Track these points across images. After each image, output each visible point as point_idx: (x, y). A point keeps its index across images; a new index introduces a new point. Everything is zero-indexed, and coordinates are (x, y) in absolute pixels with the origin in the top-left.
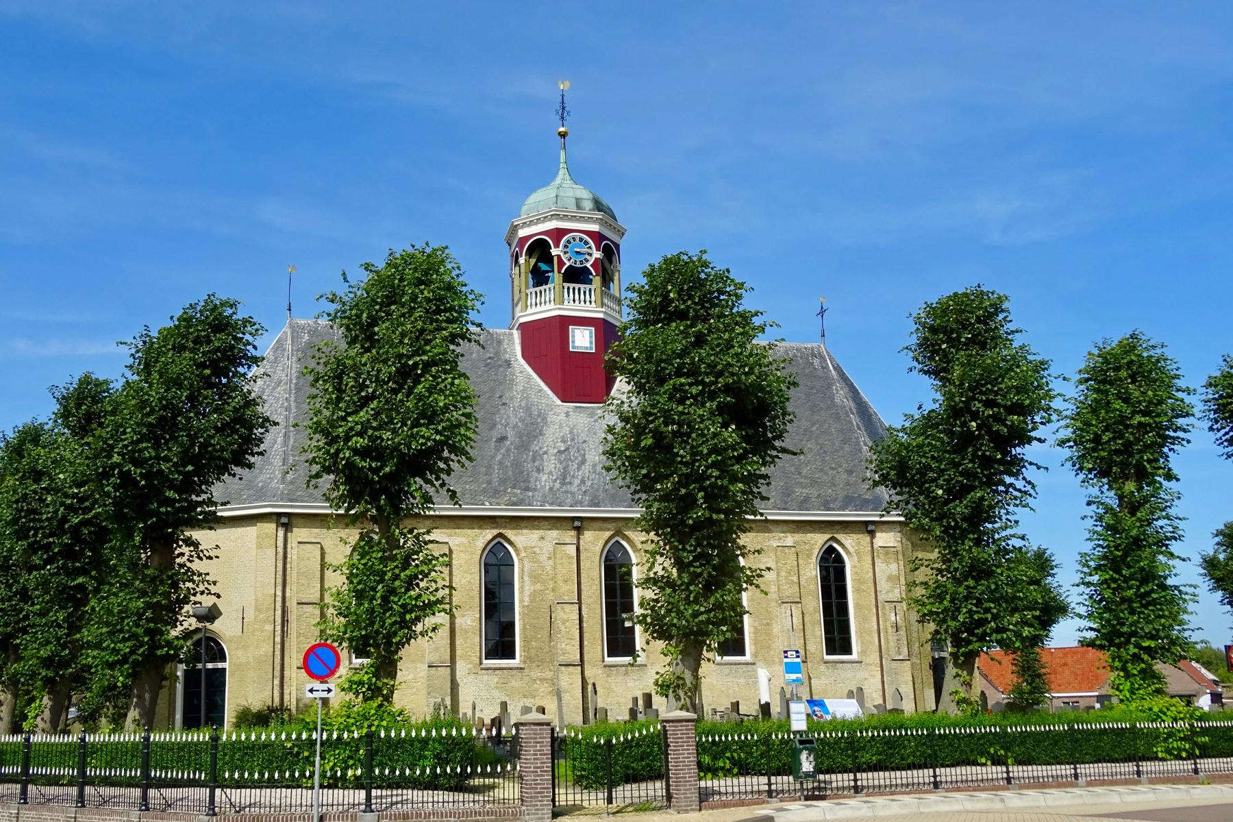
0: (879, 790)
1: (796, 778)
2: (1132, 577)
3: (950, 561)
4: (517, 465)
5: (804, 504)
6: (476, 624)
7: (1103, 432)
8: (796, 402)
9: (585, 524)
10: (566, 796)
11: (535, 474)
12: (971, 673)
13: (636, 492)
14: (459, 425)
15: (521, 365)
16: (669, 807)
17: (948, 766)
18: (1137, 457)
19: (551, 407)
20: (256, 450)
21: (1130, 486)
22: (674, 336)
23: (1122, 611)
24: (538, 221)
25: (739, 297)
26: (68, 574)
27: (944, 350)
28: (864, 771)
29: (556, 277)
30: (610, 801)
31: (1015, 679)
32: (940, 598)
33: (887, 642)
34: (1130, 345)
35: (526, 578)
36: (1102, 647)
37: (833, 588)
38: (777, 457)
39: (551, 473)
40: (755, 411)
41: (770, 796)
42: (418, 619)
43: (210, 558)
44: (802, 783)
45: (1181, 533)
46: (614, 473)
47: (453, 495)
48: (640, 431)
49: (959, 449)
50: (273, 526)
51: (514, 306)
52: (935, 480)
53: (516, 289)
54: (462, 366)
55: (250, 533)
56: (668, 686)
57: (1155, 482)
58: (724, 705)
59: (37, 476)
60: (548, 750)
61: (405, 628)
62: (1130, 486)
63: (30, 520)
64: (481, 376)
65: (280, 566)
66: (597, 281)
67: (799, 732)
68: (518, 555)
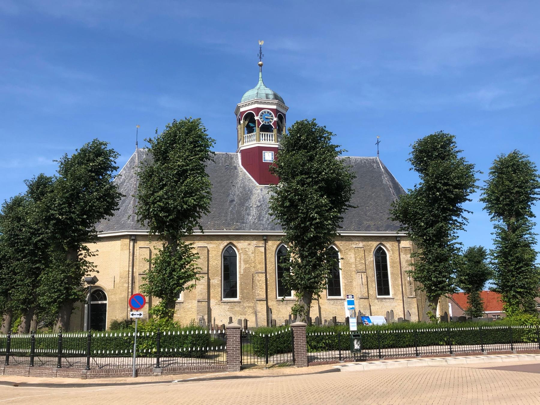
0: (391, 357)
1: (352, 352)
2: (513, 260)
3: (427, 255)
4: (239, 213)
5: (368, 229)
6: (219, 282)
7: (501, 196)
8: (355, 184)
9: (269, 238)
10: (247, 360)
11: (246, 216)
12: (436, 305)
13: (283, 225)
14: (204, 197)
15: (241, 168)
16: (294, 365)
17: (425, 346)
18: (516, 207)
19: (254, 187)
20: (115, 208)
21: (513, 220)
22: (300, 156)
23: (508, 276)
24: (249, 104)
25: (329, 139)
26: (33, 263)
27: (425, 161)
28: (386, 348)
29: (257, 129)
30: (267, 362)
31: (468, 305)
32: (422, 271)
33: (406, 288)
34: (514, 156)
35: (242, 262)
36: (499, 292)
37: (381, 265)
38: (346, 209)
39: (253, 216)
40: (336, 190)
41: (340, 360)
42: (185, 282)
43: (94, 255)
44: (355, 354)
45: (536, 241)
46: (274, 217)
47: (201, 228)
48: (285, 198)
49: (432, 205)
50: (128, 240)
51: (238, 142)
52: (421, 219)
53: (239, 135)
54: (207, 171)
55: (117, 244)
56: (297, 311)
57: (524, 218)
58: (330, 318)
59: (19, 219)
60: (238, 340)
61: (179, 286)
62: (513, 220)
63: (16, 239)
64: (223, 173)
65: (131, 258)
66: (275, 131)
67: (353, 331)
68: (238, 252)
